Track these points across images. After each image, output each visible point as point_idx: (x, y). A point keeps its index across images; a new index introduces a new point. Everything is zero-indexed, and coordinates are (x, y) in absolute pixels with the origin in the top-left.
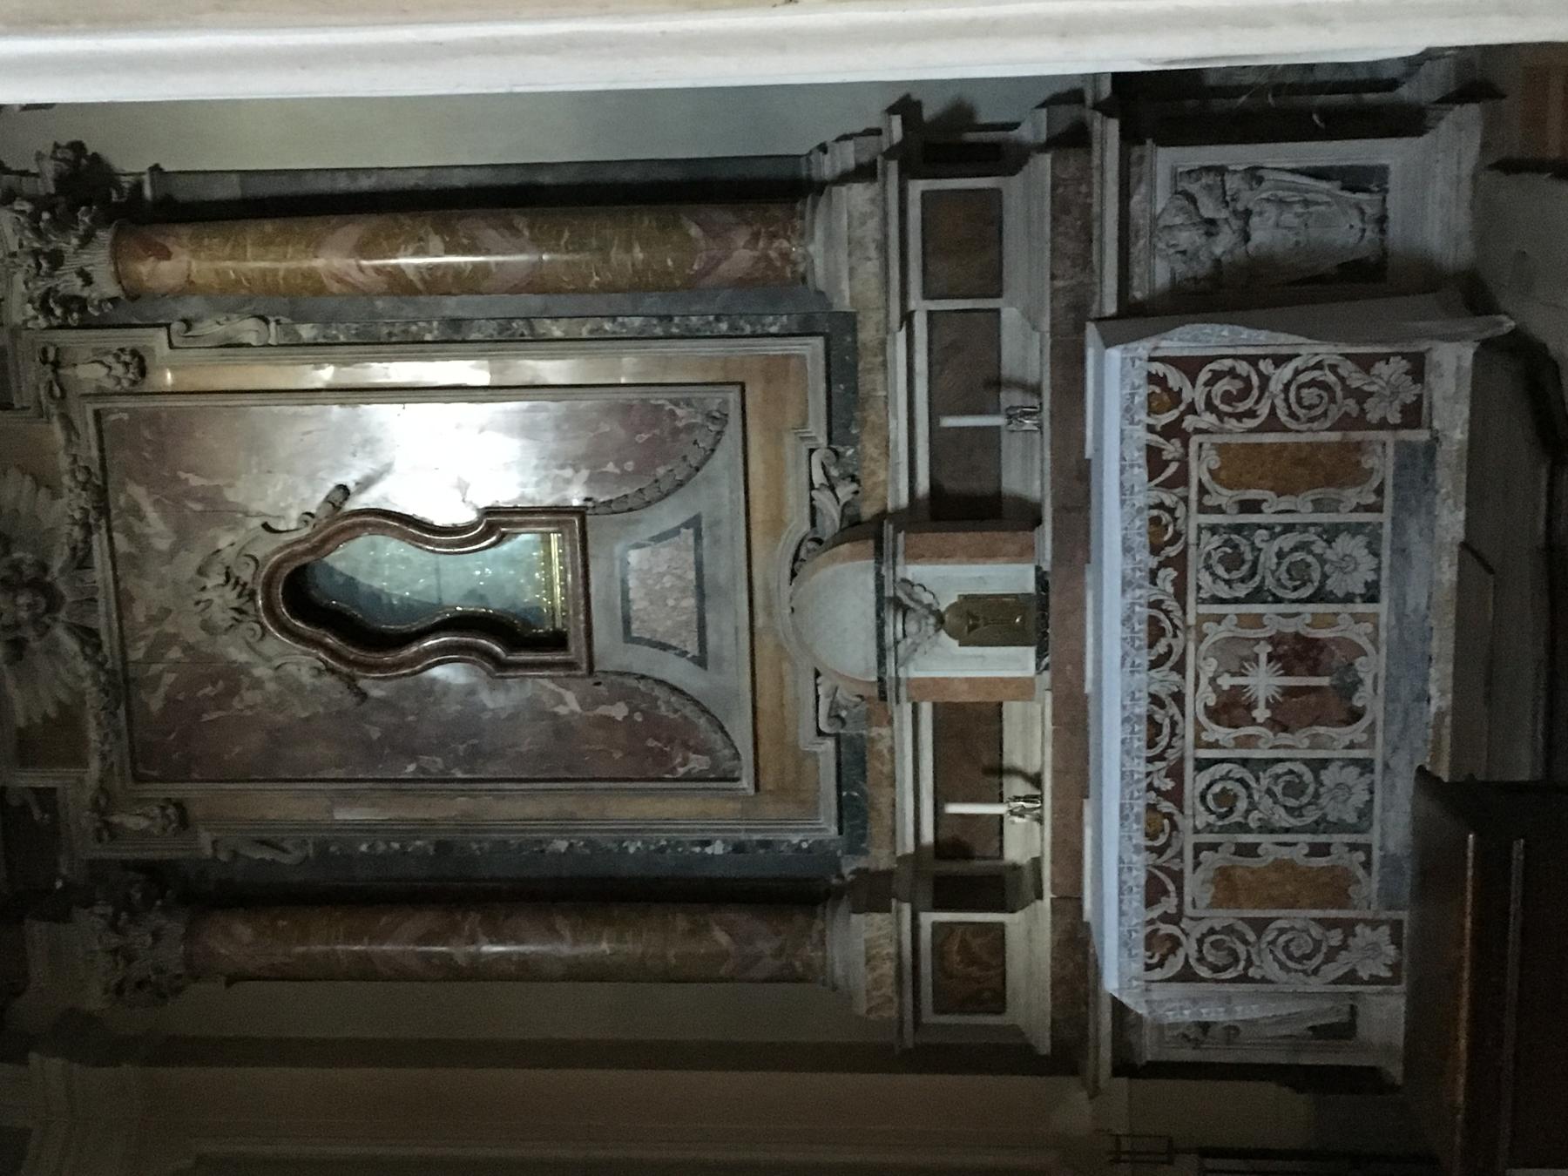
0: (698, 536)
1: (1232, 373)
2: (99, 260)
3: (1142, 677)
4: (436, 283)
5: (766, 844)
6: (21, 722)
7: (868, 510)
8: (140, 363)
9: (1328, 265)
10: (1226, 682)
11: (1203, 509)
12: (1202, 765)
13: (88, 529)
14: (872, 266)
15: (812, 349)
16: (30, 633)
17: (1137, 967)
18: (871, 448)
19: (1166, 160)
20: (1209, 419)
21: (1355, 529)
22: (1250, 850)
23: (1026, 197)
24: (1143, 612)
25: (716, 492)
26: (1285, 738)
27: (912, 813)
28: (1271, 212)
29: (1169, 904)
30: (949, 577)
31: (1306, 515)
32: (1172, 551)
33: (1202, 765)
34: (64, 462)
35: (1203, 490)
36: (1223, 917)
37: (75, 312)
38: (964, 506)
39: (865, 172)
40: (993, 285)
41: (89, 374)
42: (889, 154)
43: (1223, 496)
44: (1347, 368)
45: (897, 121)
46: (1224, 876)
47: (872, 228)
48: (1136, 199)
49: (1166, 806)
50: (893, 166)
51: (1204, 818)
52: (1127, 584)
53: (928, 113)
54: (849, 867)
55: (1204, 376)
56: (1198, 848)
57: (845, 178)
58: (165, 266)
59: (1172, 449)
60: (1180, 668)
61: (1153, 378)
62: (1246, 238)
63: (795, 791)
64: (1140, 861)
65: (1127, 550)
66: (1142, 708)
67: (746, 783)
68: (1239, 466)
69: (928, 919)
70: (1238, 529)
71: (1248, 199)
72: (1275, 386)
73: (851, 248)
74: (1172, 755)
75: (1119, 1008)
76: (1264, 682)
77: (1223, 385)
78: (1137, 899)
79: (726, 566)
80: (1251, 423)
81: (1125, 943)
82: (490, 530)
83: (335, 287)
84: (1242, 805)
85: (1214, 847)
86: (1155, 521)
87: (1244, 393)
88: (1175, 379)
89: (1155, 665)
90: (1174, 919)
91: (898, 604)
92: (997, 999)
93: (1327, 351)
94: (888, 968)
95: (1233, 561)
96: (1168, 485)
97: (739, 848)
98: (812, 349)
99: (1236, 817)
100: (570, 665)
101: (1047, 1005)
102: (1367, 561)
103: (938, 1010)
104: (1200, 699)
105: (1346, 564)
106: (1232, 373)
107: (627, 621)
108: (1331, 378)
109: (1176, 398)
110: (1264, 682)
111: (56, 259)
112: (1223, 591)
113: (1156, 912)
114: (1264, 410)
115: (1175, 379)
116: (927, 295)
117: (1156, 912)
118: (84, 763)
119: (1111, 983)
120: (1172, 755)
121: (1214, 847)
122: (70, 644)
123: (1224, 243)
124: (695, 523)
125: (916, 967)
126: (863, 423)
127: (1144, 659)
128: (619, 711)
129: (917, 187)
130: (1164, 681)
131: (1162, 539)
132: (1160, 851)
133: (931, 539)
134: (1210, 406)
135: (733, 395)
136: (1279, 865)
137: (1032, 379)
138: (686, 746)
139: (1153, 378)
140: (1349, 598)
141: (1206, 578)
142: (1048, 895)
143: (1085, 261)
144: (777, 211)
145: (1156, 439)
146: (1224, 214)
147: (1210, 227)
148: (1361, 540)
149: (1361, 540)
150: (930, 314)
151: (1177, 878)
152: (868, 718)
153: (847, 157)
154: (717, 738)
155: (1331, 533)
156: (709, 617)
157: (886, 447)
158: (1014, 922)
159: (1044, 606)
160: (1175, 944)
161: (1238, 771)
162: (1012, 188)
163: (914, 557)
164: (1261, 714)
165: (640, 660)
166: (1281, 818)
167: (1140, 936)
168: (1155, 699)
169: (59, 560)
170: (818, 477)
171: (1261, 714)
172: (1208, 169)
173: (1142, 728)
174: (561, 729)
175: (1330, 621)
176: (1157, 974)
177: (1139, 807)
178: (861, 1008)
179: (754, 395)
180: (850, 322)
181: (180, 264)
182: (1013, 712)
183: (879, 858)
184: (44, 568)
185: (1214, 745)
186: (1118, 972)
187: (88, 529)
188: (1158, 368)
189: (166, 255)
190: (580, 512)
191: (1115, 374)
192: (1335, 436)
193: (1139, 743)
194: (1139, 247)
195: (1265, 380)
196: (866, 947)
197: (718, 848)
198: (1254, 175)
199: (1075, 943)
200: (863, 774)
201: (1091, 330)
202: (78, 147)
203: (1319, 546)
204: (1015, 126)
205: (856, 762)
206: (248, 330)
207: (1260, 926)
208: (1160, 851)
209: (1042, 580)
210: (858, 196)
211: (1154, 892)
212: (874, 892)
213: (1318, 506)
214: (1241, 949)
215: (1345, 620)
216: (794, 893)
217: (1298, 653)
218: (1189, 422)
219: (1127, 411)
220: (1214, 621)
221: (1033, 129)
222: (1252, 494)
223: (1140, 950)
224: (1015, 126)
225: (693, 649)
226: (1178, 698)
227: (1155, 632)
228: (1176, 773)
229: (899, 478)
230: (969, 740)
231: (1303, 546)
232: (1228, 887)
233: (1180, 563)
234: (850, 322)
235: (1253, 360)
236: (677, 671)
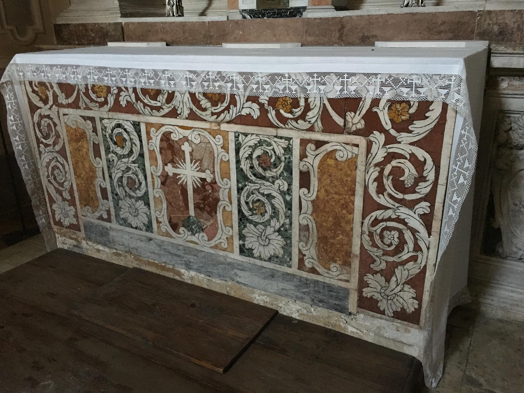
1: (421, 178)
9: (502, 222)
10: (186, 148)
11: (304, 143)
12: (136, 125)
17: (29, 76)
20: (380, 155)
21: (287, 247)
29: (62, 99)
31: (298, 219)
32: (272, 115)
33: (136, 125)
35: (319, 144)
43: (313, 161)
44: (413, 269)
52: (247, 76)
55: (421, 154)
59: (355, 120)
60: (193, 116)
61: (425, 106)
65: (273, 77)
68: (338, 176)
70: (289, 169)
72: (404, 212)
74: (139, 106)
76: (189, 174)
80: (373, 188)
81: (38, 69)
84: (119, 150)
87: (399, 186)
88: (421, 128)
93: (431, 259)
95: (265, 162)
96: (325, 115)
99: (113, 147)
106: (421, 178)
108: (405, 256)
109: (402, 127)
110: (189, 174)
112: (244, 153)
114: (382, 200)
115: (421, 128)
127: (197, 89)
130: (183, 103)
131: (283, 107)
139: (425, 106)
140: (242, 237)
141: (252, 141)
151: (75, 105)
155: (284, 233)
164: (170, 169)
168: (171, 96)
171: (170, 169)
173: (151, 85)
177: (107, 81)
192: (356, 250)
195: (411, 205)
207: (62, 152)
215: (228, 231)
218: (378, 138)
226: (174, 114)
227: (215, 99)
228: (130, 109)
231: (275, 214)
232: (78, 137)
233: (263, 121)
235: (430, 197)
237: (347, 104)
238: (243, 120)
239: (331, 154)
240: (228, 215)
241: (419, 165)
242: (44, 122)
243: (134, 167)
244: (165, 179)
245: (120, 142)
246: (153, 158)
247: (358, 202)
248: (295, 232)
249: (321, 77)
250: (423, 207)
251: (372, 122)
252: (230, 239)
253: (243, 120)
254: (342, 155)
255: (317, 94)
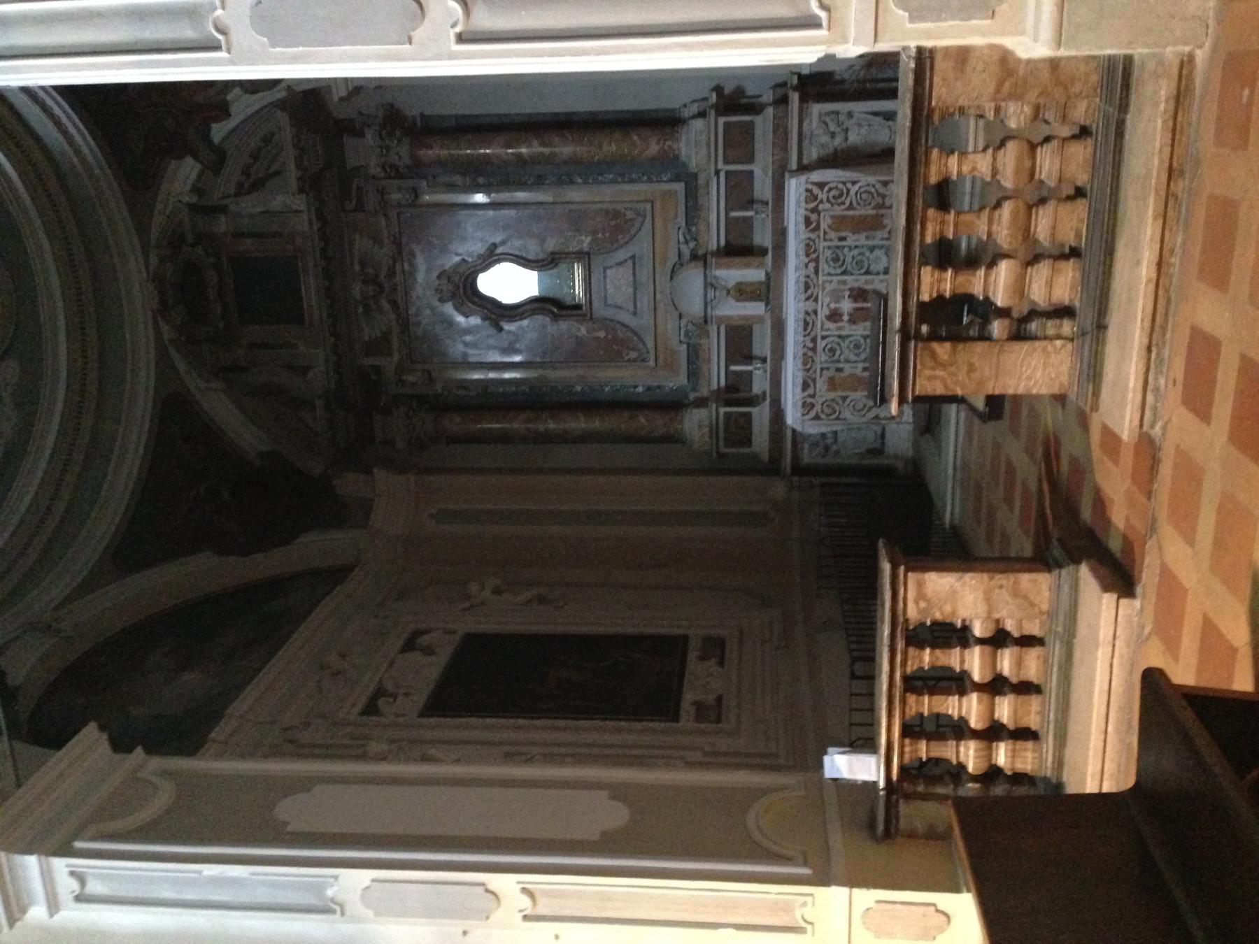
0: (634, 264)
1: (836, 188)
2: (404, 150)
3: (801, 304)
4: (535, 160)
5: (659, 387)
6: (367, 338)
7: (701, 252)
8: (415, 192)
9: (877, 149)
10: (833, 306)
11: (825, 240)
12: (823, 338)
13: (395, 261)
14: (704, 152)
15: (679, 187)
16: (372, 303)
17: (799, 415)
18: (702, 228)
19: (816, 109)
20: (828, 206)
21: (881, 247)
22: (839, 370)
23: (763, 124)
24: (803, 279)
25: (641, 246)
26: (854, 327)
27: (716, 373)
28: (856, 128)
29: (811, 391)
30: (734, 274)
31: (863, 241)
32: (814, 256)
33: (823, 338)
34: (385, 233)
35: (825, 233)
36: (831, 395)
37: (395, 172)
38: (739, 249)
39: (702, 115)
40: (750, 158)
41: (395, 197)
42: (711, 107)
43: (833, 235)
44: (878, 186)
45: (714, 95)
46: (831, 379)
47: (704, 138)
48: (805, 124)
49: (810, 353)
50: (713, 112)
51: (824, 358)
52: (797, 269)
53: (727, 91)
54: (692, 396)
55: (826, 189)
56: (822, 369)
57: (693, 117)
58: (430, 152)
59: (814, 217)
60: (816, 300)
61: (807, 190)
62: (847, 139)
63: (670, 366)
64: (800, 375)
65: (797, 255)
66: (802, 316)
67: (652, 363)
68: (840, 223)
69: (723, 410)
70: (838, 247)
71: (848, 124)
72: (852, 192)
73: (697, 144)
74: (813, 334)
75: (794, 431)
76: (847, 306)
77: (833, 193)
78: (799, 389)
79: (645, 275)
80: (843, 207)
81: (794, 405)
82: (553, 260)
83: (495, 161)
84: (838, 352)
85: (828, 369)
86: (807, 245)
87: (841, 195)
88: (816, 190)
89: (807, 299)
90: (813, 396)
91: (712, 285)
92: (748, 442)
93: (871, 179)
94: (706, 430)
95: (836, 260)
96: (813, 230)
97: (649, 389)
98: (679, 187)
99: (836, 357)
100: (585, 315)
101: (767, 443)
102: (884, 259)
103: (726, 446)
104: (823, 312)
105: (877, 259)
106: (836, 188)
107: (606, 298)
108: (873, 190)
109: (816, 198)
110: (847, 306)
111: (388, 149)
112: (832, 271)
113: (806, 394)
114: (848, 203)
115: (816, 190)
116: (726, 161)
117: (806, 394)
118: (390, 355)
119: (789, 420)
120: (813, 334)
121: (828, 369)
122: (386, 306)
123: (838, 141)
124: (633, 257)
125: (717, 427)
126: (699, 217)
127: (803, 297)
128: (602, 334)
129: (722, 120)
130: (810, 305)
131: (809, 249)
132: (808, 370)
133: (726, 260)
134: (828, 200)
135: (648, 206)
136: (852, 376)
137: (765, 199)
138: (628, 348)
139: (807, 190)
140: (878, 273)
141: (826, 266)
142: (768, 400)
143: (785, 149)
144: (668, 130)
145: (808, 213)
146: (838, 130)
147: (833, 135)
148: (883, 251)
149: (883, 251)
150: (727, 173)
151: (814, 381)
152: (700, 337)
153: (695, 109)
154: (641, 345)
155: (872, 249)
156: (638, 296)
157: (708, 225)
158: (754, 411)
159: (768, 287)
160: (813, 406)
161: (837, 340)
162: (758, 120)
163: (719, 266)
164: (846, 318)
165: (608, 313)
166: (852, 357)
167: (800, 403)
168: (807, 313)
169: (383, 273)
170: (682, 239)
171: (846, 318)
172: (832, 112)
173: (802, 324)
174: (580, 342)
175: (871, 282)
176: (806, 417)
177: (800, 354)
178: (696, 446)
179: (658, 205)
180: (695, 176)
181: (435, 152)
182: (756, 328)
183: (704, 392)
184: (377, 276)
185: (828, 330)
186: (792, 417)
187: (395, 261)
188: (810, 187)
189: (431, 148)
190: (588, 254)
191: (795, 188)
192: (873, 212)
193: (801, 329)
194: (806, 142)
195: (848, 191)
196: (695, 423)
197: (640, 389)
198: (850, 115)
199: (778, 415)
200: (698, 357)
201: (787, 175)
202: (391, 105)
203: (867, 254)
204: (759, 96)
205: (694, 355)
206: (458, 180)
207: (844, 399)
208: (808, 370)
209: (767, 274)
210: (699, 124)
211: (805, 386)
212: (702, 403)
213: (867, 238)
214: (837, 408)
215: (876, 282)
216: (673, 405)
217: (859, 294)
218: (821, 207)
219: (798, 203)
220: (829, 281)
221: (768, 97)
222: (844, 234)
223: (800, 408)
224: (759, 96)
225: (631, 308)
226: (815, 312)
227: (807, 287)
228: (814, 340)
229: (714, 237)
230: (739, 341)
231: (862, 254)
232: (832, 384)
233: (817, 260)
234: (695, 176)
235: (844, 183)
236: (624, 317)
237: (808, 222)
238: (817, 272)
239: (830, 227)
240: (867, 282)
241: (830, 189)
242: (827, 410)
243: (847, 342)
244: (853, 321)
245: (832, 351)
246: (840, 328)
247: (851, 213)
248: (871, 243)
249: (796, 233)
250: (849, 185)
251: (814, 210)
252: (882, 281)
253: (817, 272)
254: (829, 221)
255: (804, 235)
